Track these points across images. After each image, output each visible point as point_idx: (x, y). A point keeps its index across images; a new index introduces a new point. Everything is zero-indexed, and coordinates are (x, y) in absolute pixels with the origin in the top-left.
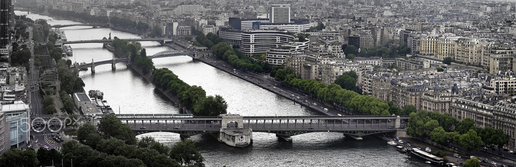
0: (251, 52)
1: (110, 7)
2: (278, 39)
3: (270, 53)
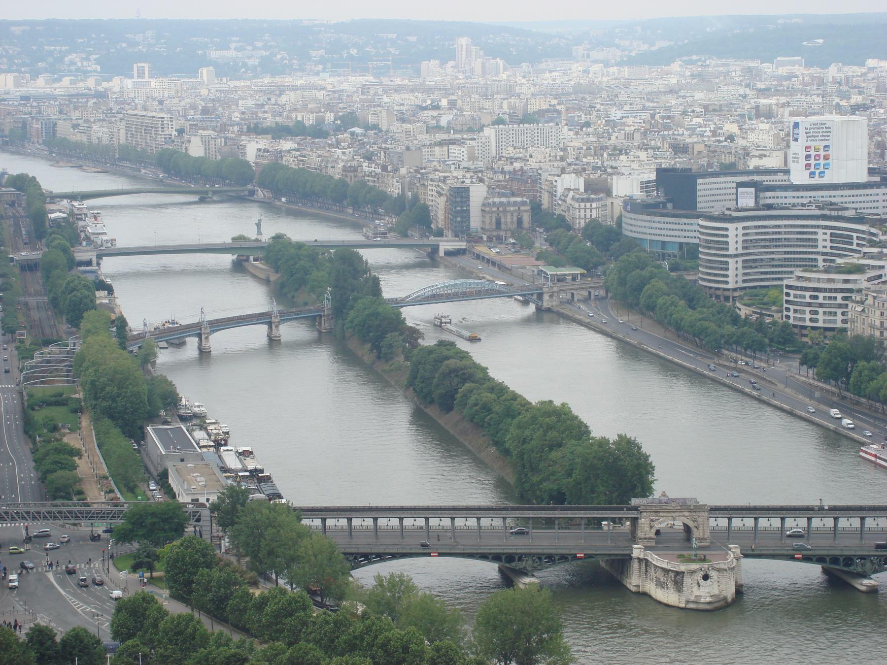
0: (731, 286)
1: (257, 130)
2: (823, 240)
3: (796, 288)
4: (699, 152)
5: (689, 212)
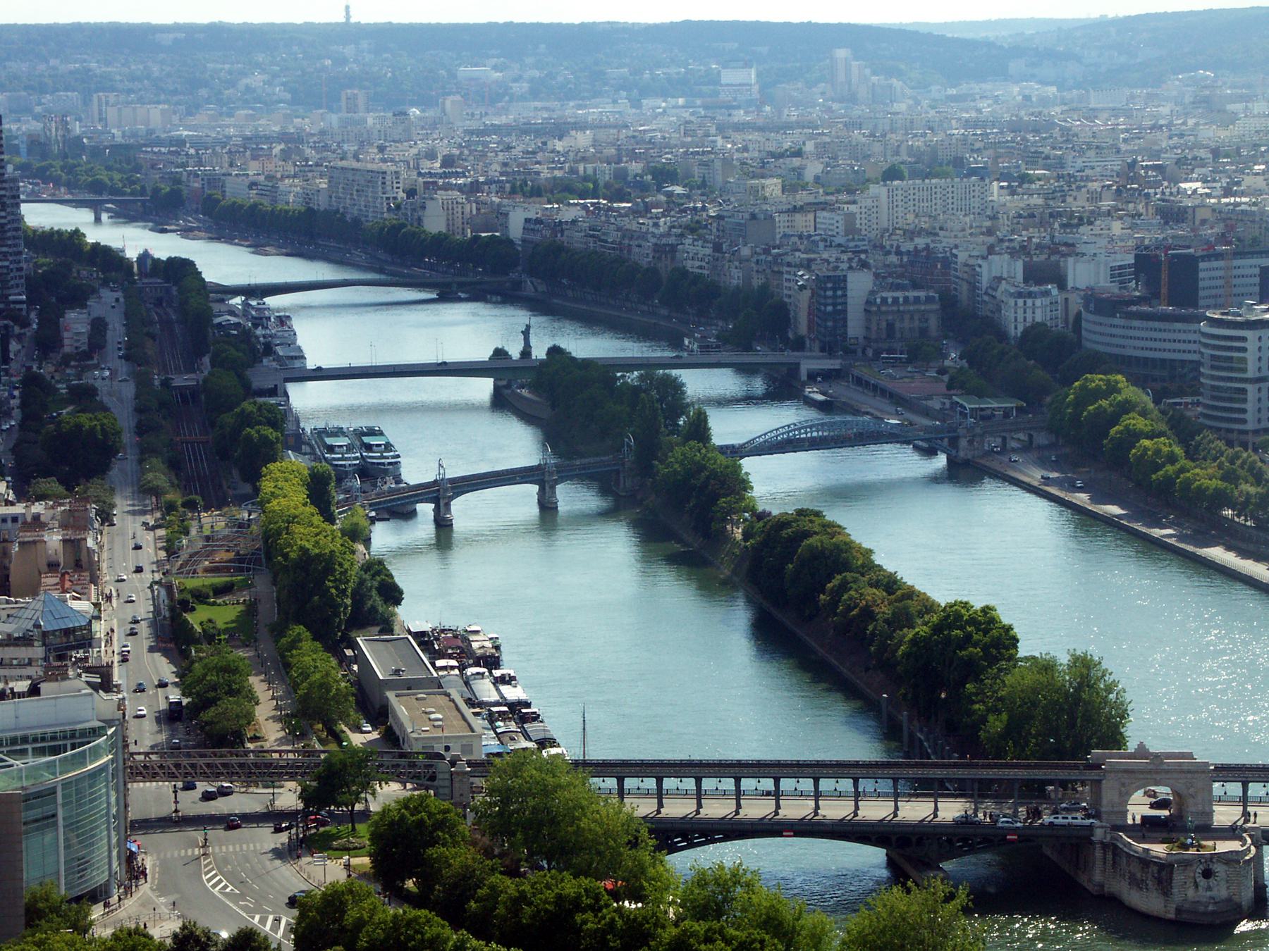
0: (1250, 426)
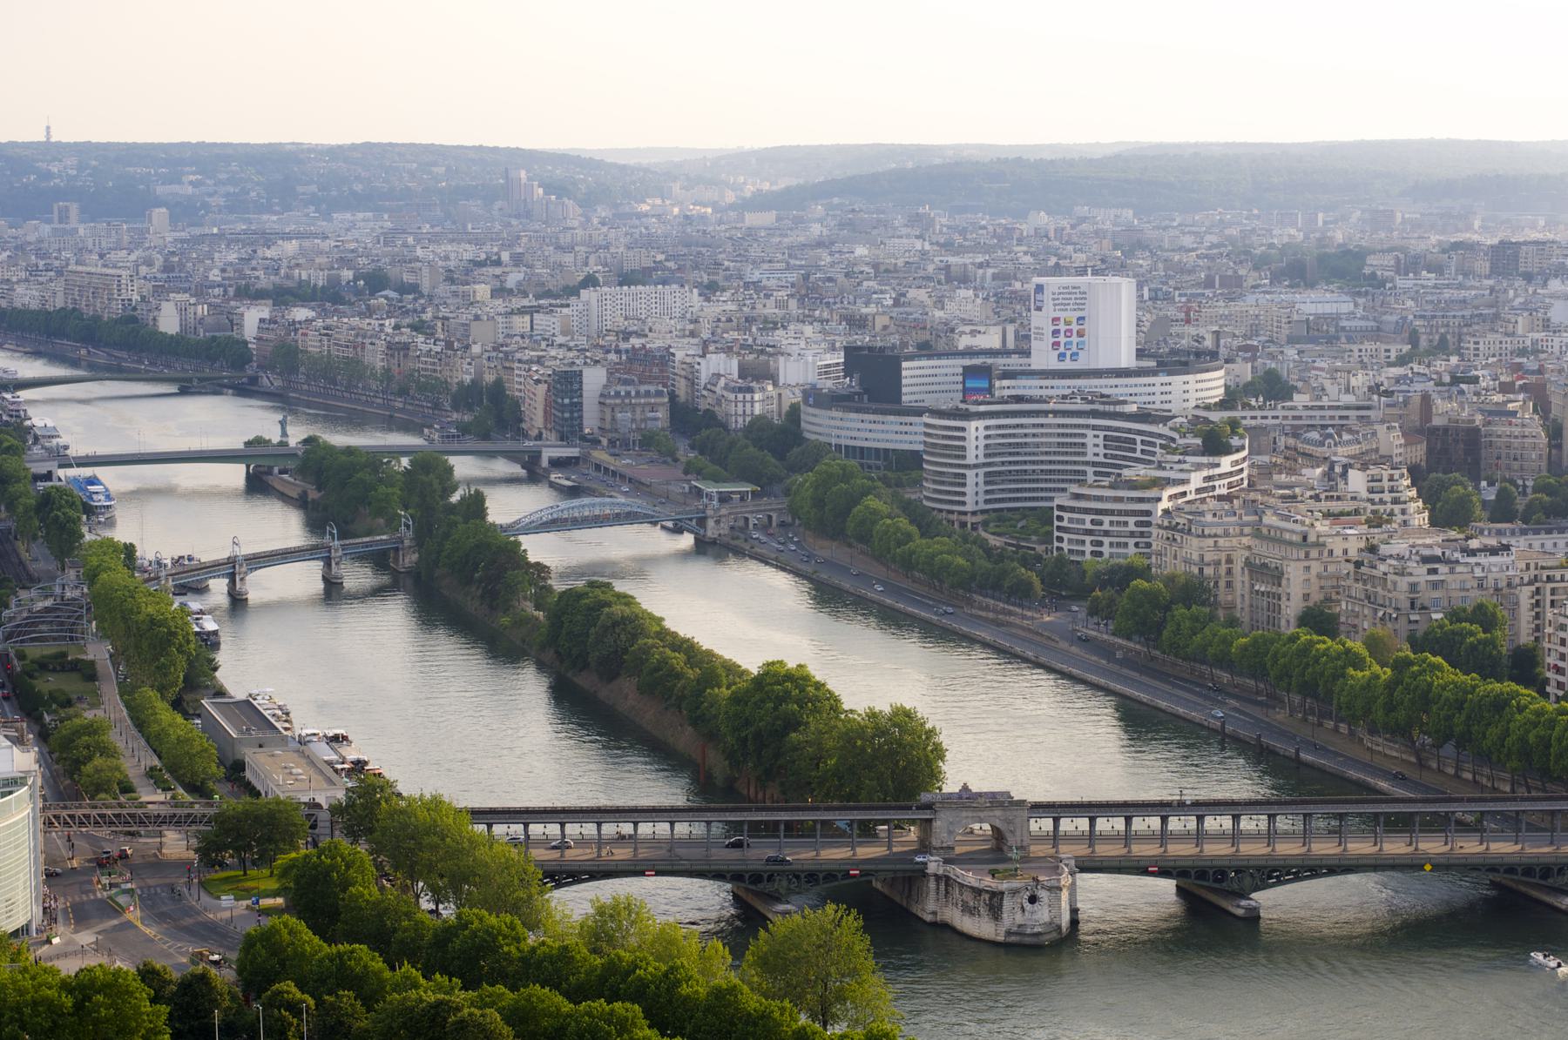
0: (969, 508)
1: (250, 294)
2: (1094, 445)
3: (1072, 510)
4: (885, 327)
5: (889, 407)
